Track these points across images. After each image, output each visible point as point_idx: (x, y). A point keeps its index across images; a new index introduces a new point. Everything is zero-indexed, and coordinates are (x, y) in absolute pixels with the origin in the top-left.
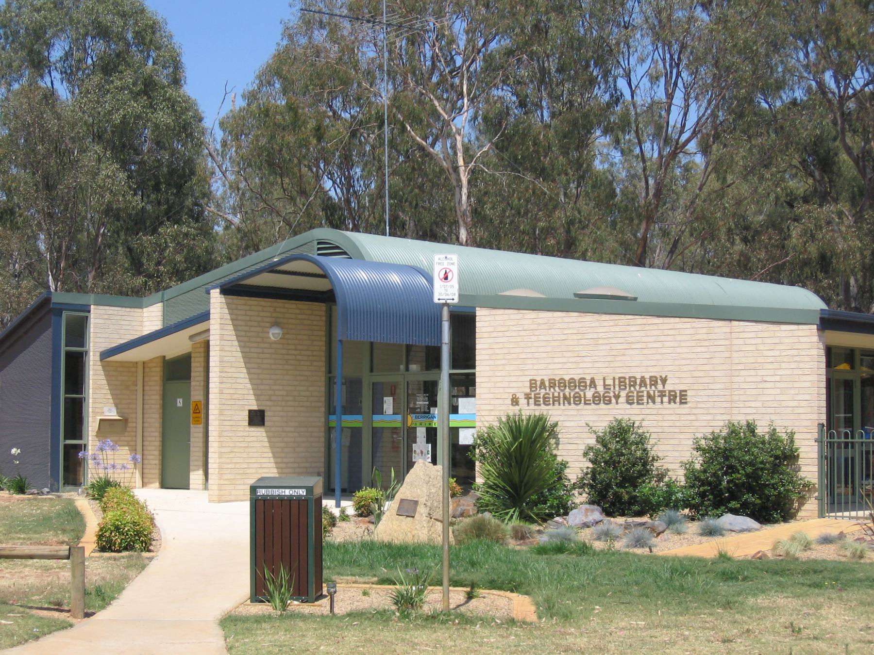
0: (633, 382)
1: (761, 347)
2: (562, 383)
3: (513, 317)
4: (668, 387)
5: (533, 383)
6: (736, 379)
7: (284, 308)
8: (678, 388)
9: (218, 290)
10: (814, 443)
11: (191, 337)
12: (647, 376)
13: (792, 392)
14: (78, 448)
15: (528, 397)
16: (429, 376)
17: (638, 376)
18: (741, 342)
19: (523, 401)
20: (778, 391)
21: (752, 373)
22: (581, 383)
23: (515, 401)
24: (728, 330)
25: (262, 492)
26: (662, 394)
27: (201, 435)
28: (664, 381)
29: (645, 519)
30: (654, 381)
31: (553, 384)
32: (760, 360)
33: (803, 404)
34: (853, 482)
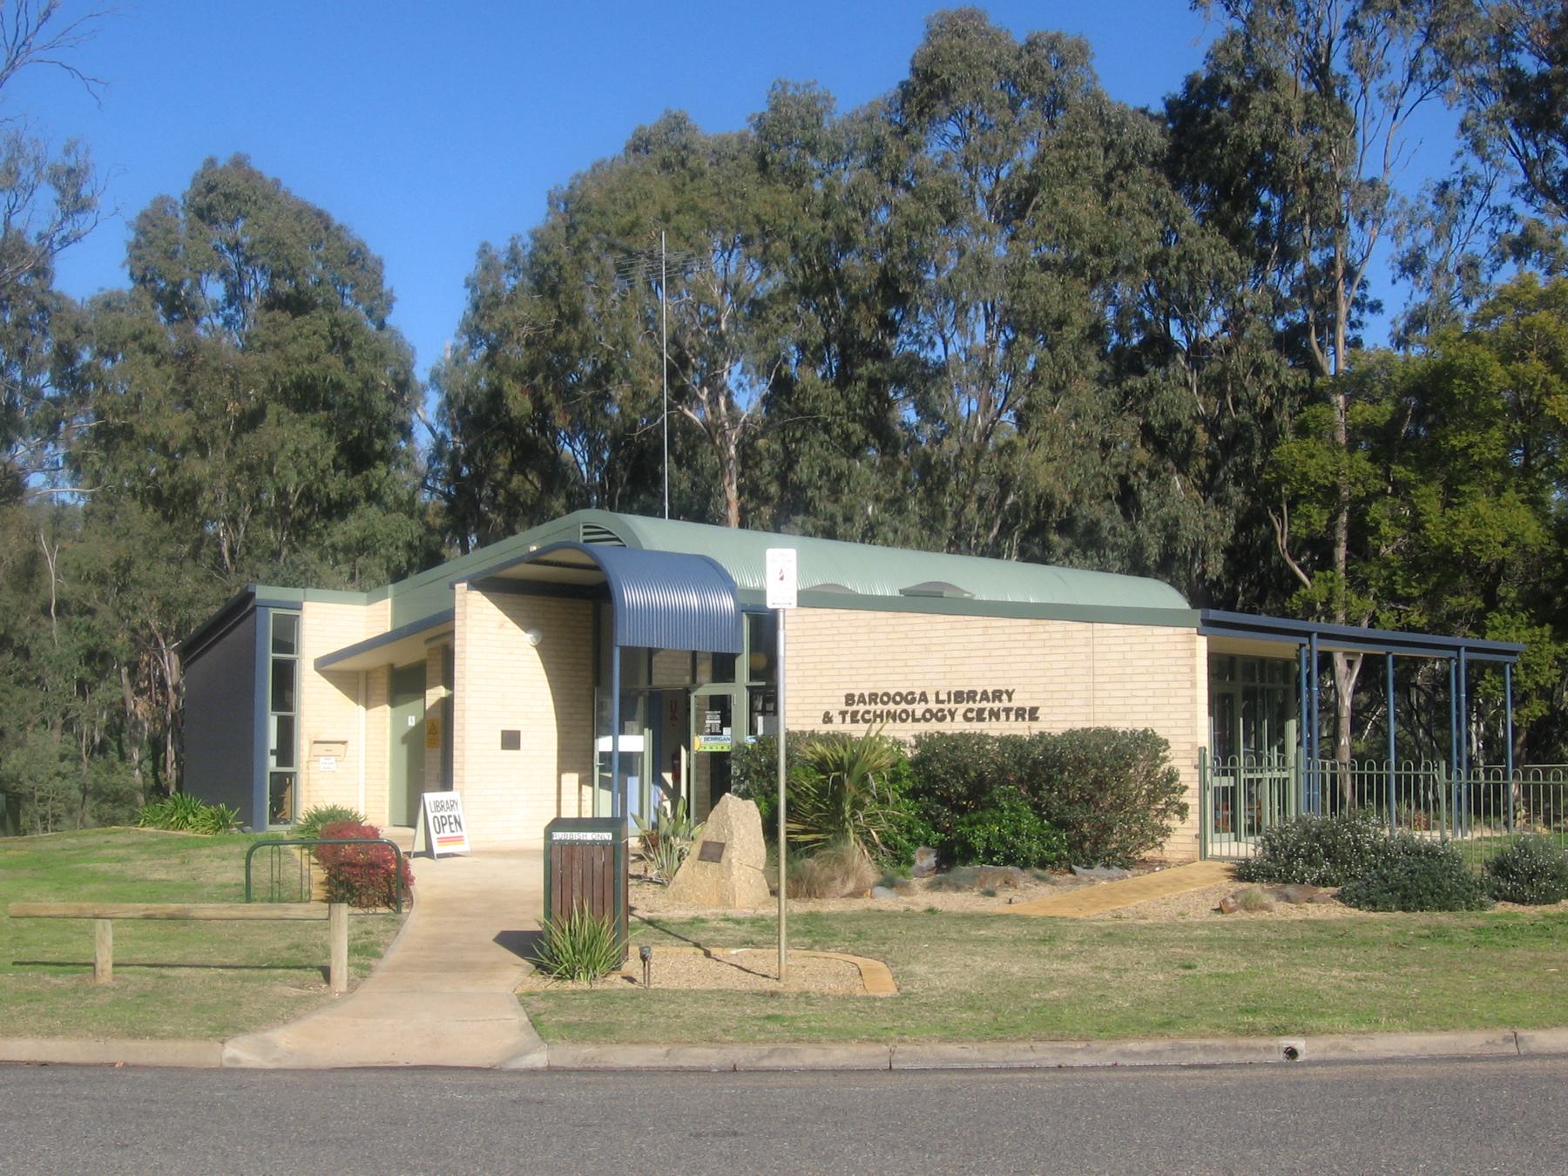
0: (971, 695)
1: (1129, 655)
2: (888, 698)
3: (825, 618)
4: (1015, 704)
5: (850, 699)
6: (1098, 694)
7: (1237, 1049)
8: (1028, 705)
9: (465, 585)
10: (1192, 770)
11: (428, 641)
12: (990, 691)
13: (1168, 708)
14: (291, 775)
15: (843, 713)
16: (719, 689)
17: (980, 691)
18: (1105, 649)
19: (837, 719)
20: (1150, 708)
21: (1119, 686)
22: (908, 698)
23: (827, 718)
24: (1089, 634)
25: (558, 836)
26: (1008, 711)
27: (438, 760)
28: (1010, 695)
29: (582, 984)
30: (997, 695)
31: (873, 698)
32: (1128, 670)
33: (1180, 723)
34: (1388, 793)
